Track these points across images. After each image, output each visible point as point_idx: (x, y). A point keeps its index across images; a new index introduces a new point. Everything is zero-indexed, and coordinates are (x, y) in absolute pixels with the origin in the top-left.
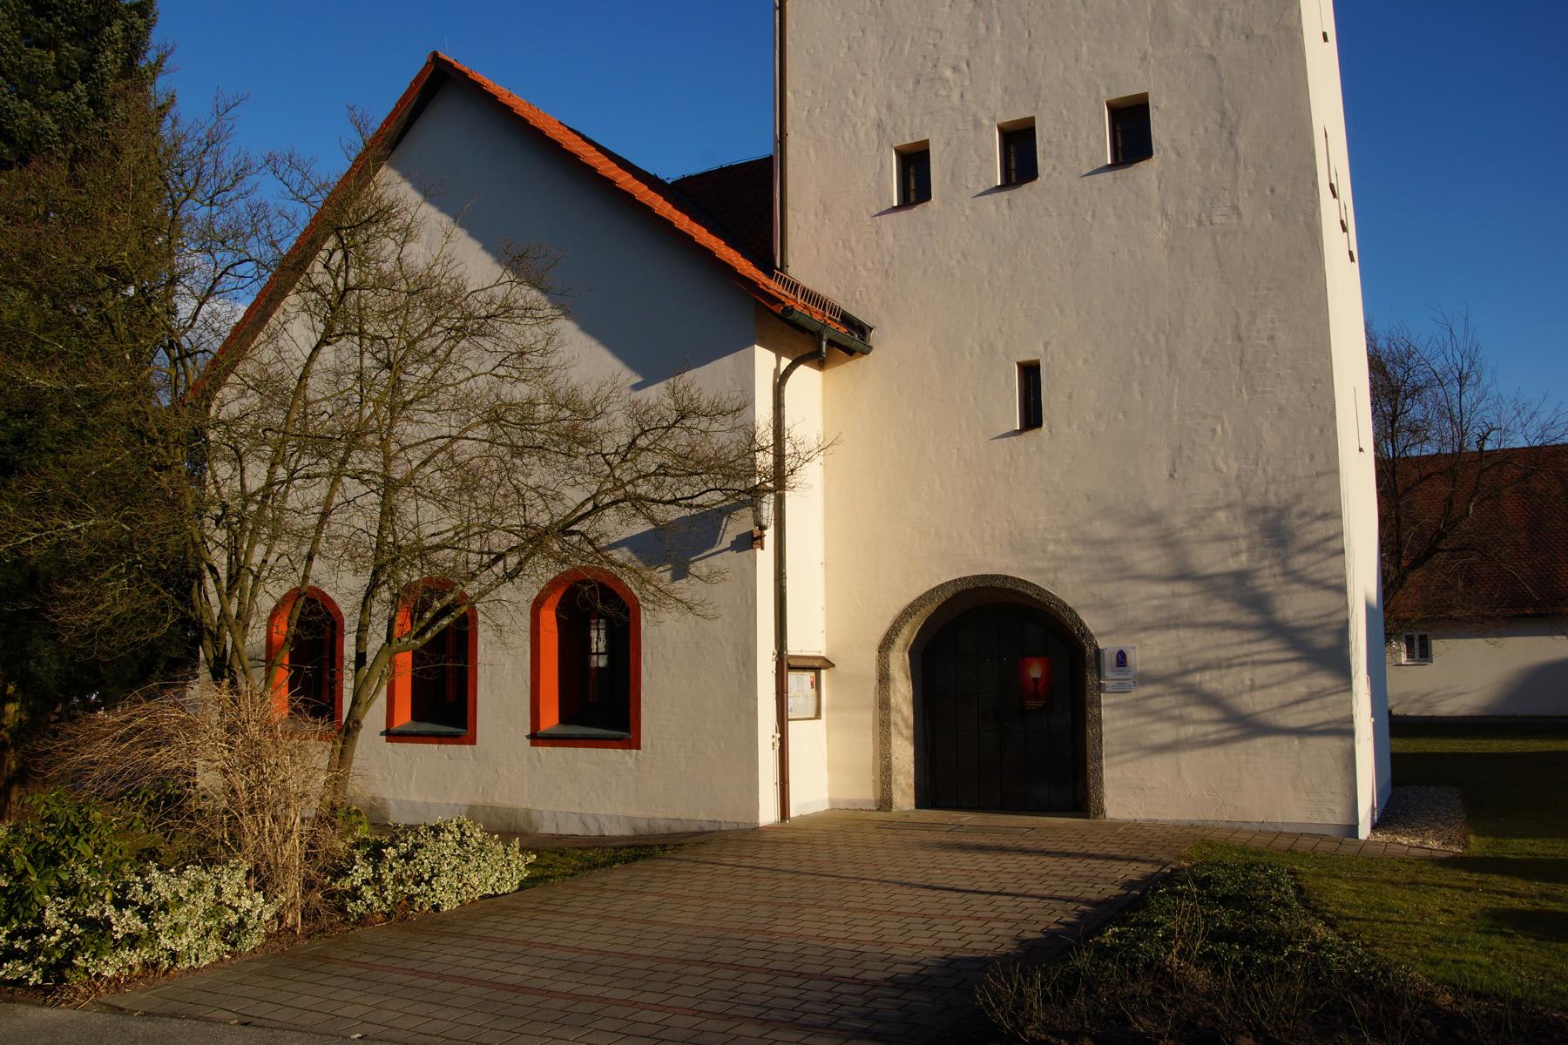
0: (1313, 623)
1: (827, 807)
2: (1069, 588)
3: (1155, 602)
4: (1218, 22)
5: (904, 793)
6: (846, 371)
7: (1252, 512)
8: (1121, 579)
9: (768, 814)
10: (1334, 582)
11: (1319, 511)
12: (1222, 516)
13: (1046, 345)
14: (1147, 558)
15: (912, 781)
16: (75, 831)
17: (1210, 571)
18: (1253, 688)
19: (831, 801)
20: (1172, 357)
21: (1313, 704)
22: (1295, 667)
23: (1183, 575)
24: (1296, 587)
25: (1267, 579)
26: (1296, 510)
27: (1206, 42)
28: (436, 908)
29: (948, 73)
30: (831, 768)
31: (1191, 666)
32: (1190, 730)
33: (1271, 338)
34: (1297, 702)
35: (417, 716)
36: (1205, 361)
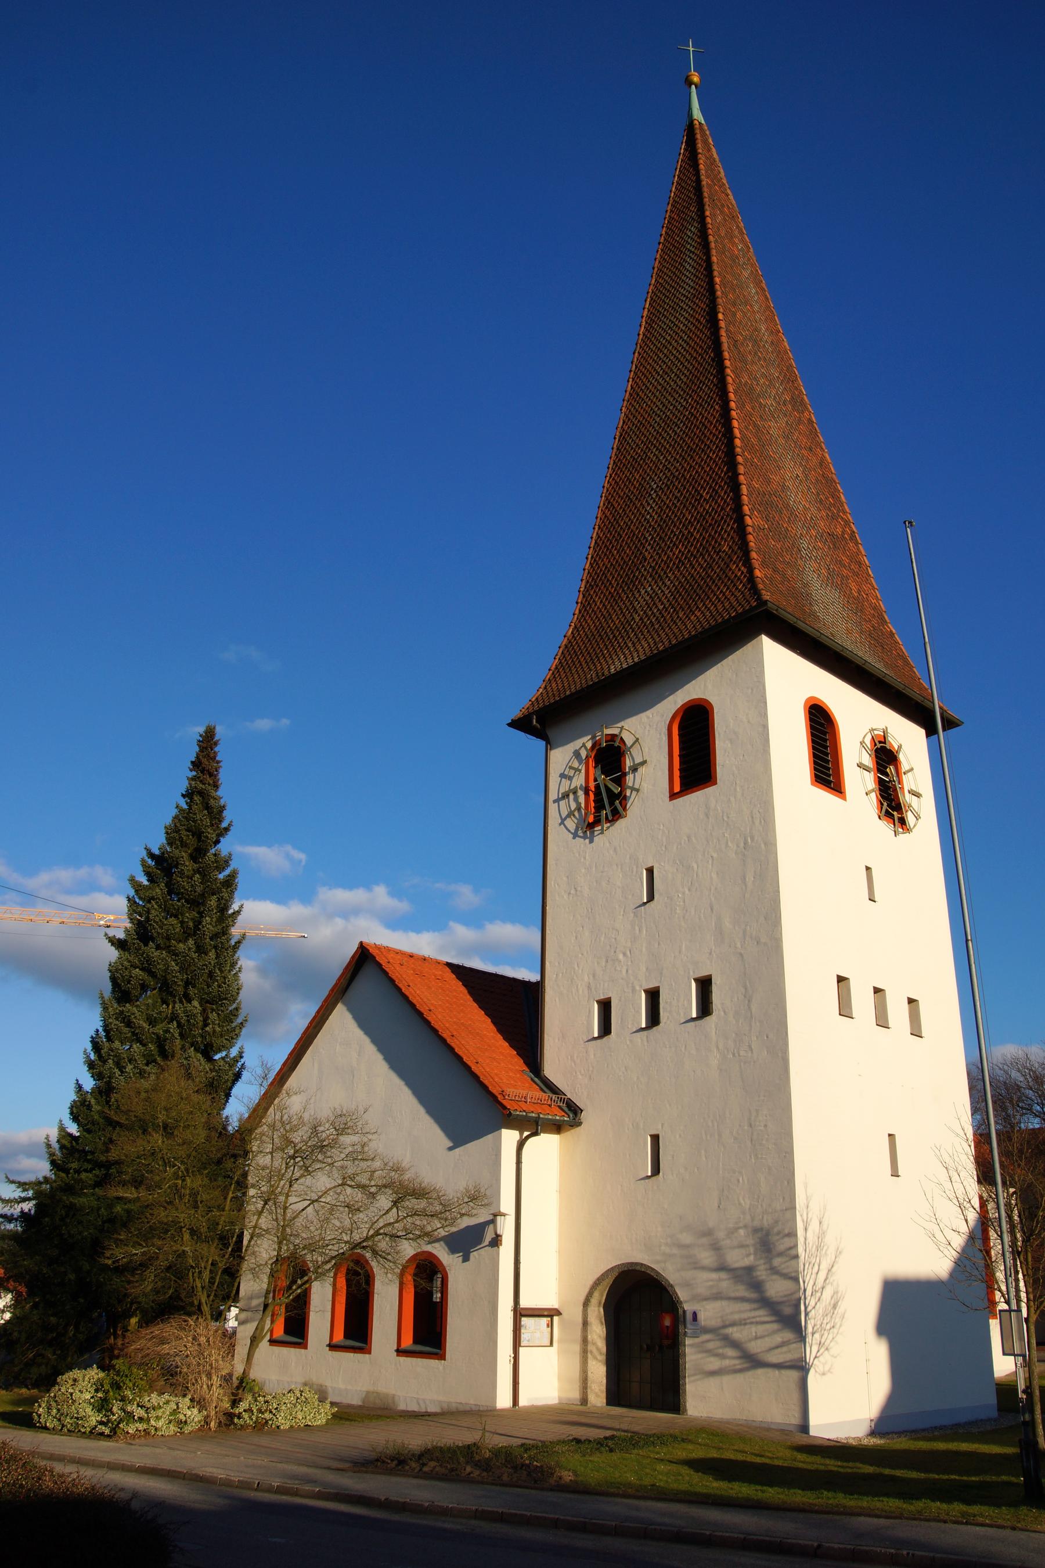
0: (785, 1299)
1: (556, 1401)
2: (671, 1273)
3: (711, 1283)
4: (745, 932)
5: (597, 1395)
6: (570, 1135)
7: (756, 1230)
8: (695, 1268)
9: (503, 1400)
10: (793, 1275)
11: (786, 1231)
12: (742, 1232)
13: (663, 1125)
14: (707, 1257)
15: (604, 1388)
16: (127, 1376)
17: (737, 1265)
18: (756, 1338)
19: (560, 1398)
20: (720, 1135)
21: (785, 1349)
22: (775, 1326)
23: (722, 1268)
24: (775, 1277)
25: (762, 1273)
26: (775, 1230)
27: (739, 945)
28: (278, 1427)
29: (621, 956)
30: (559, 1379)
31: (727, 1323)
32: (727, 1362)
33: (765, 1126)
34: (777, 1347)
35: (347, 1336)
36: (735, 1139)
